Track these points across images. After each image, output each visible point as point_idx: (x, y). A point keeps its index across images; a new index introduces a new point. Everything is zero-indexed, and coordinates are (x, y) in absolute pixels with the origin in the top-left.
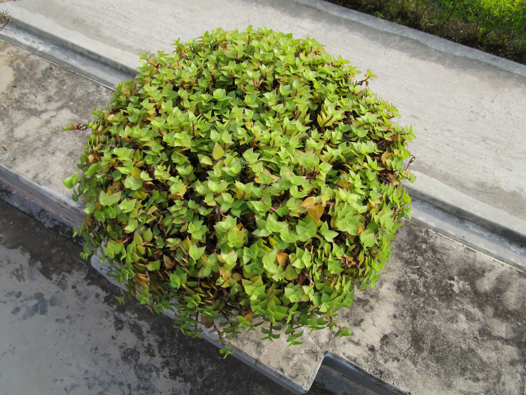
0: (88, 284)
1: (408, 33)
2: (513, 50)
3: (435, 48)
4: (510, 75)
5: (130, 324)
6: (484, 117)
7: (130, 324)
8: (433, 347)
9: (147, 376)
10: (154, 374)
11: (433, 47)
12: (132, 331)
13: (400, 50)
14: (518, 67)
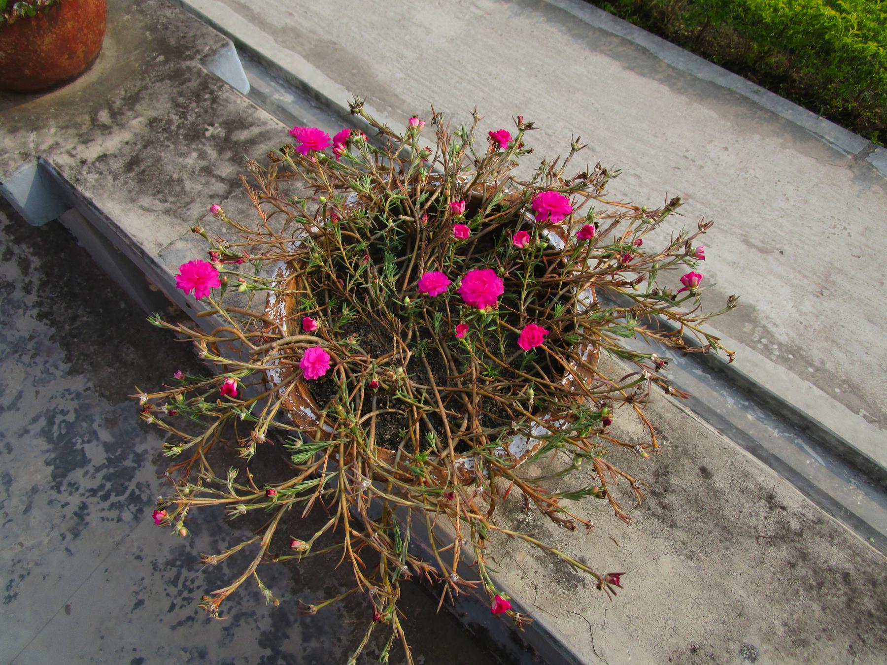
1: (636, 35)
2: (804, 89)
3: (670, 62)
4: (774, 116)
5: (20, 258)
6: (702, 167)
7: (20, 258)
8: (144, 171)
9: (12, 312)
10: (21, 311)
11: (666, 61)
12: (19, 265)
14: (792, 109)
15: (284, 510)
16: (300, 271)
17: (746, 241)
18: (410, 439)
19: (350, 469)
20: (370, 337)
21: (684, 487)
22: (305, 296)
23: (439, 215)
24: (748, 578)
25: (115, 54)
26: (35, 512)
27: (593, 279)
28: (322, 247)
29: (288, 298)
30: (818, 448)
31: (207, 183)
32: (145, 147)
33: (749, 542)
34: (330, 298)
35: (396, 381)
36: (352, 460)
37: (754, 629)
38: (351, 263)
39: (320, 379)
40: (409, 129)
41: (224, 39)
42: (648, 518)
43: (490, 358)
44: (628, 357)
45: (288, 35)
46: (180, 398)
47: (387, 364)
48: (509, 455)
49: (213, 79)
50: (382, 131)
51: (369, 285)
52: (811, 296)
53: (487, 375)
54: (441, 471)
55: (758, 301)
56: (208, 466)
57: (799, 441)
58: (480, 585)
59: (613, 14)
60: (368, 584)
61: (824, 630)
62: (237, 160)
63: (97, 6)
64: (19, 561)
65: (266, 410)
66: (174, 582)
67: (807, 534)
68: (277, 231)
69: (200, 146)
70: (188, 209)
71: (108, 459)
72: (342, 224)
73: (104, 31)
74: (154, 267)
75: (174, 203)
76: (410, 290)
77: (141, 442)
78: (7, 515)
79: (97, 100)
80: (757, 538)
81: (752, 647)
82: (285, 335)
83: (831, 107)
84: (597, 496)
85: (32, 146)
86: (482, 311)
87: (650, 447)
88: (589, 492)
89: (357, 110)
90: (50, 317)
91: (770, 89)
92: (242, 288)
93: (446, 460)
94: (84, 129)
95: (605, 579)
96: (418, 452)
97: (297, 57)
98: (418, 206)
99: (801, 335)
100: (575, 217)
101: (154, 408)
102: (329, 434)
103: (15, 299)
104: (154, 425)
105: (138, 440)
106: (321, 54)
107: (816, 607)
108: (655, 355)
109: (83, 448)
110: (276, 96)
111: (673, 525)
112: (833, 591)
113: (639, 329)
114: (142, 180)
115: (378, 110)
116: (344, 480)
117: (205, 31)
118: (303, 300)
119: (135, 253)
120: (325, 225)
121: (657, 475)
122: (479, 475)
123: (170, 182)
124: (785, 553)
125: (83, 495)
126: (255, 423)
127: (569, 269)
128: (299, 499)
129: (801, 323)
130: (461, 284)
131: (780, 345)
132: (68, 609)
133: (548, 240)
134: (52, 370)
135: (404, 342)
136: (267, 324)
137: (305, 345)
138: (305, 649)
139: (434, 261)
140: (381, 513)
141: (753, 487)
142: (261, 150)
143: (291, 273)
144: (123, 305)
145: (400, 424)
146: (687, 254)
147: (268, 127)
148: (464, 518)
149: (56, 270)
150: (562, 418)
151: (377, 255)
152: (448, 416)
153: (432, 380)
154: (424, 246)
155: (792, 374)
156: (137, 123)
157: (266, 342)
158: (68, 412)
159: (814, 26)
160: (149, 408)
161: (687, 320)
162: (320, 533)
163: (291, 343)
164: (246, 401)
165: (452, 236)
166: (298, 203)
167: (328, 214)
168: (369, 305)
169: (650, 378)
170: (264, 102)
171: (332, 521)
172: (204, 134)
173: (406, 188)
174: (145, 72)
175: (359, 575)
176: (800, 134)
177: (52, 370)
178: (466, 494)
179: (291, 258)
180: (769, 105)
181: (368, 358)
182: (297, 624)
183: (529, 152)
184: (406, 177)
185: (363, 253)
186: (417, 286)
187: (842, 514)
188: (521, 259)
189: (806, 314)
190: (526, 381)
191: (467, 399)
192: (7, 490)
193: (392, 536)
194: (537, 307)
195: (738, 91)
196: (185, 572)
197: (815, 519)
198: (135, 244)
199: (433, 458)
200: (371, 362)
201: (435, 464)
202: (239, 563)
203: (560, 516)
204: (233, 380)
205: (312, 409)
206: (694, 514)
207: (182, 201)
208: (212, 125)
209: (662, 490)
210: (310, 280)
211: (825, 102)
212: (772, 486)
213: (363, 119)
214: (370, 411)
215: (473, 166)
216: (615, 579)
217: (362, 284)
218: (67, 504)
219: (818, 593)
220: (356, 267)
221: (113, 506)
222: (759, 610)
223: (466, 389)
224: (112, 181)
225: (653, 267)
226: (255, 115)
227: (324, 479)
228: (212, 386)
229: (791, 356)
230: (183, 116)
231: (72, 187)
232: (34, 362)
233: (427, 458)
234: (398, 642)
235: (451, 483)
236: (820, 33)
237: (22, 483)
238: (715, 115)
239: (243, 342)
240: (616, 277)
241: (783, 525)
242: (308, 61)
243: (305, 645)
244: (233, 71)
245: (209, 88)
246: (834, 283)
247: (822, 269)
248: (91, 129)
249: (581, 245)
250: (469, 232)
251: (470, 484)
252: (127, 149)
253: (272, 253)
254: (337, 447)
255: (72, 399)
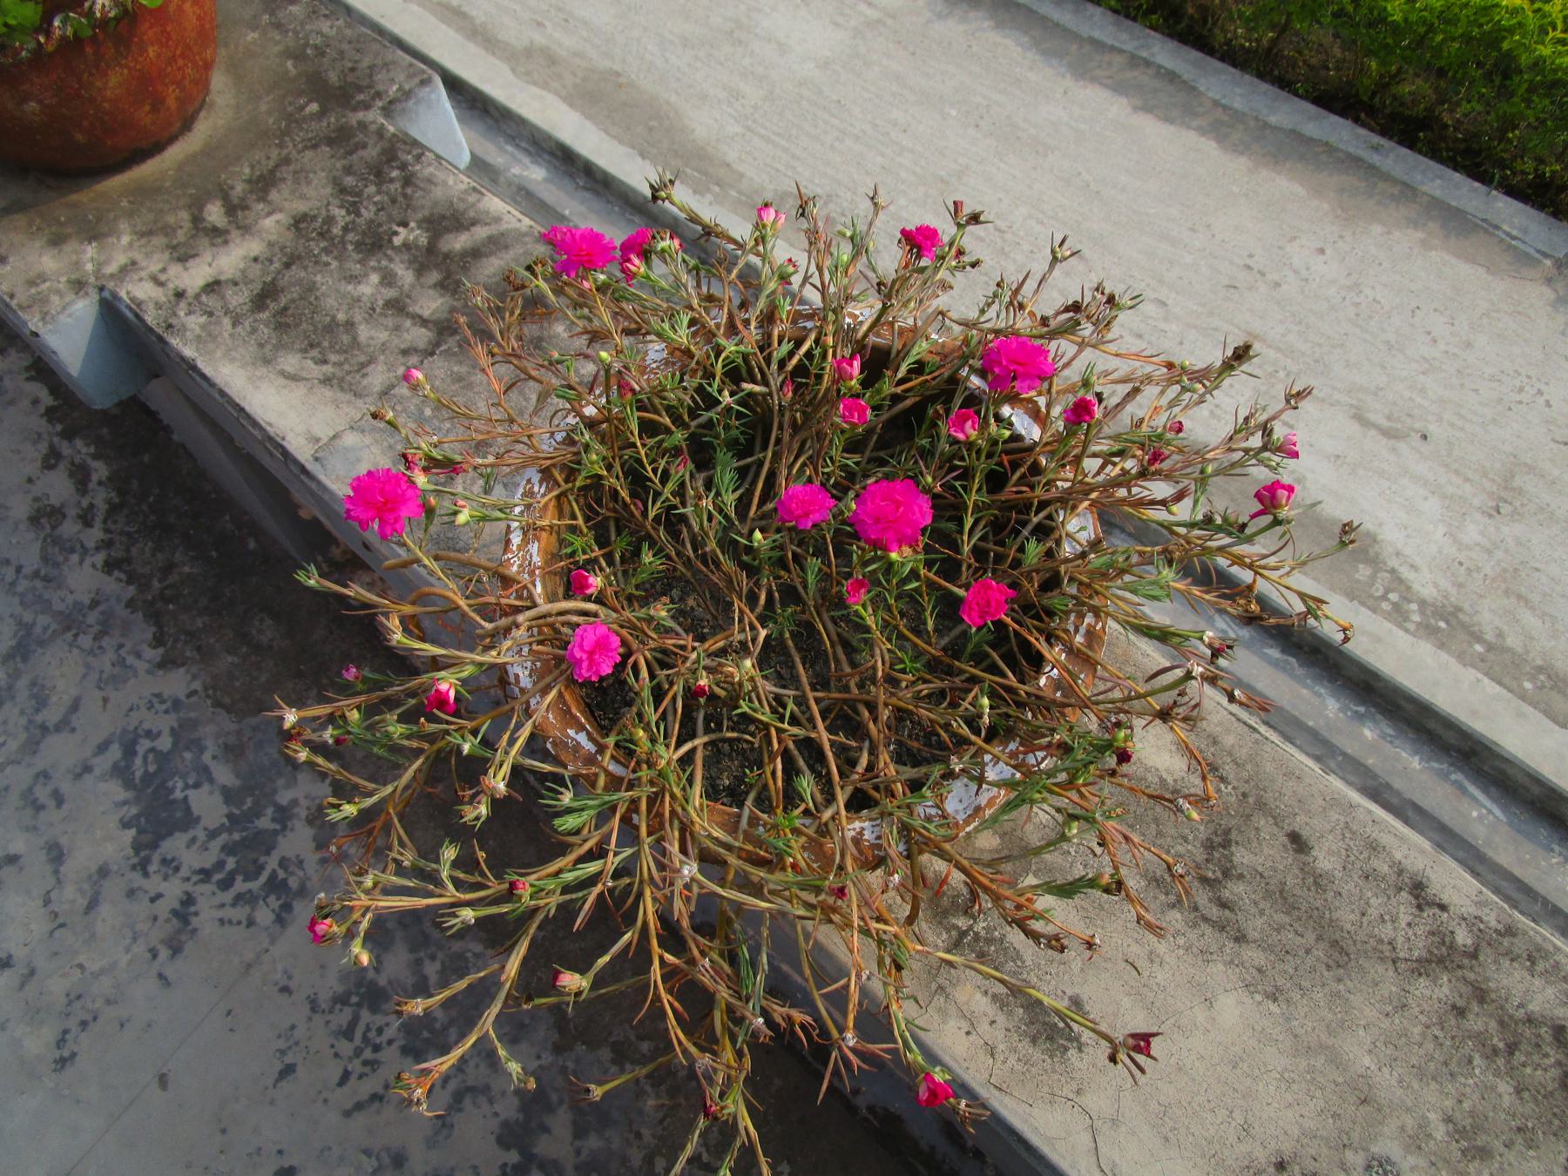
0: (28, 379)
2: (1464, 140)
3: (1217, 97)
4: (1408, 191)
5: (73, 464)
6: (1277, 285)
7: (73, 464)
8: (285, 309)
9: (60, 559)
11: (1210, 94)
12: (71, 475)
13: (1114, 90)
14: (1441, 177)
15: (540, 917)
16: (564, 486)
17: (1360, 418)
18: (765, 787)
19: (659, 841)
20: (691, 602)
21: (1260, 869)
22: (574, 529)
23: (812, 380)
24: (1378, 1033)
25: (233, 102)
26: (105, 910)
27: (1094, 495)
28: (602, 442)
29: (544, 535)
30: (1493, 789)
31: (397, 328)
32: (287, 266)
33: (1381, 969)
34: (619, 533)
35: (741, 684)
36: (662, 826)
37: (1390, 1127)
38: (655, 471)
39: (602, 679)
40: (757, 226)
41: (424, 72)
42: (1195, 925)
43: (907, 639)
44: (1162, 636)
45: (536, 62)
46: (354, 715)
47: (723, 652)
48: (945, 817)
49: (405, 143)
50: (708, 231)
51: (689, 510)
52: (1478, 516)
53: (903, 671)
54: (821, 845)
55: (1380, 525)
56: (405, 837)
57: (1457, 776)
58: (895, 1052)
59: (1115, 11)
60: (693, 1049)
61: (1519, 1129)
62: (448, 285)
63: (199, 18)
64: (79, 997)
65: (506, 737)
66: (348, 1033)
67: (1486, 955)
68: (521, 413)
69: (384, 263)
70: (364, 376)
71: (230, 816)
72: (638, 401)
73: (213, 61)
74: (306, 480)
75: (340, 364)
76: (763, 517)
77: (287, 787)
78: (56, 915)
79: (200, 187)
80: (1394, 962)
81: (1388, 1160)
82: (540, 601)
83: (1514, 173)
84: (1107, 890)
85: (89, 267)
86: (894, 556)
87: (1201, 801)
88: (1092, 883)
89: (663, 194)
90: (125, 566)
91: (1400, 143)
92: (462, 518)
93: (831, 826)
94: (181, 236)
95: (1124, 1044)
96: (779, 811)
97: (551, 98)
98: (774, 366)
99: (1461, 586)
100: (1058, 383)
101: (308, 734)
102: (621, 779)
103: (66, 536)
104: (310, 764)
105: (281, 782)
106: (598, 94)
107: (1505, 1087)
108: (1210, 634)
109: (186, 798)
110: (516, 170)
111: (1240, 938)
112: (1536, 1058)
113: (1178, 585)
114: (282, 325)
115: (695, 192)
116: (647, 862)
117: (389, 57)
118: (570, 537)
119: (271, 455)
120: (608, 402)
121: (1209, 846)
122: (891, 852)
123: (331, 328)
124: (1445, 990)
125: (188, 879)
126: (487, 760)
127: (1051, 476)
128: (568, 897)
129: (1461, 564)
130: (854, 506)
131: (1423, 603)
132: (163, 1081)
133: (1011, 424)
134: (130, 660)
135: (752, 611)
136: (507, 581)
137: (575, 619)
138: (578, 1152)
139: (804, 465)
140: (712, 920)
141: (1385, 869)
142: (492, 267)
143: (549, 490)
144: (252, 545)
145: (747, 759)
146: (1265, 448)
147: (504, 227)
148: (865, 932)
149: (135, 484)
150: (1041, 748)
151: (701, 454)
152: (832, 743)
153: (804, 680)
154: (786, 437)
155: (1444, 656)
156: (272, 224)
157: (506, 615)
158: (159, 734)
159: (1481, 26)
160: (299, 734)
161: (1264, 568)
162: (607, 958)
163: (550, 615)
164: (471, 720)
165: (838, 420)
166: (559, 362)
167: (613, 381)
168: (689, 546)
169: (1202, 675)
170: (495, 181)
171: (627, 937)
172: (390, 241)
173: (753, 333)
174: (286, 133)
175: (676, 1032)
176: (1456, 222)
177: (130, 660)
178: (869, 887)
179: (549, 462)
180: (1398, 172)
181: (688, 641)
182: (565, 1107)
183: (973, 265)
184: (753, 314)
185: (676, 452)
186: (775, 510)
187: (1538, 907)
188: (962, 459)
189: (1469, 548)
190: (974, 680)
191: (867, 714)
192: (56, 872)
193: (733, 959)
194: (991, 546)
195: (1342, 146)
196: (366, 1016)
197: (1500, 927)
198: (271, 439)
199: (808, 821)
200: (694, 649)
201: (811, 832)
202: (466, 1011)
203: (1037, 926)
204: (447, 683)
205: (588, 734)
206: (1280, 917)
207: (354, 361)
208: (405, 224)
209: (1219, 874)
210: (582, 501)
211: (1503, 165)
212: (1421, 867)
213: (675, 210)
214: (693, 736)
215: (873, 292)
216: (1142, 1042)
217: (675, 507)
218: (160, 896)
219: (1508, 1062)
220: (665, 478)
221: (238, 899)
222: (1399, 1092)
223: (865, 697)
224: (229, 327)
225: (1202, 472)
226: (481, 205)
227: (612, 862)
228: (412, 694)
229: (1442, 624)
230: (354, 209)
231: (161, 339)
232: (100, 647)
233: (797, 823)
234: (748, 1151)
235: (841, 868)
236: (1494, 39)
237: (82, 860)
238: (1300, 190)
239: (464, 615)
240: (1135, 490)
241: (1442, 937)
242: (571, 105)
243: (578, 1143)
244: (440, 128)
245: (397, 159)
246: (1520, 491)
247: (1498, 465)
248: (193, 237)
249: (1071, 433)
250: (869, 412)
251: (874, 868)
252: (256, 270)
253: (513, 454)
254: (634, 802)
255: (167, 712)
